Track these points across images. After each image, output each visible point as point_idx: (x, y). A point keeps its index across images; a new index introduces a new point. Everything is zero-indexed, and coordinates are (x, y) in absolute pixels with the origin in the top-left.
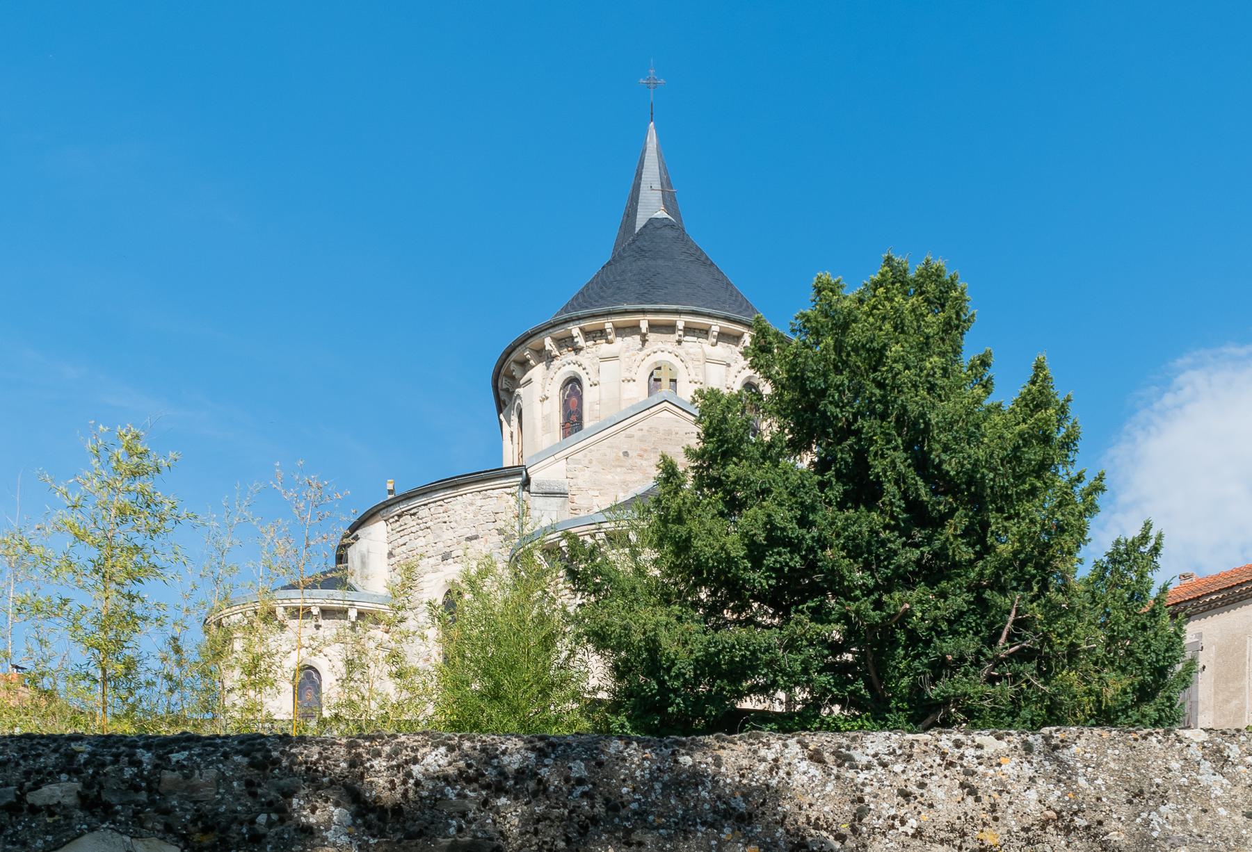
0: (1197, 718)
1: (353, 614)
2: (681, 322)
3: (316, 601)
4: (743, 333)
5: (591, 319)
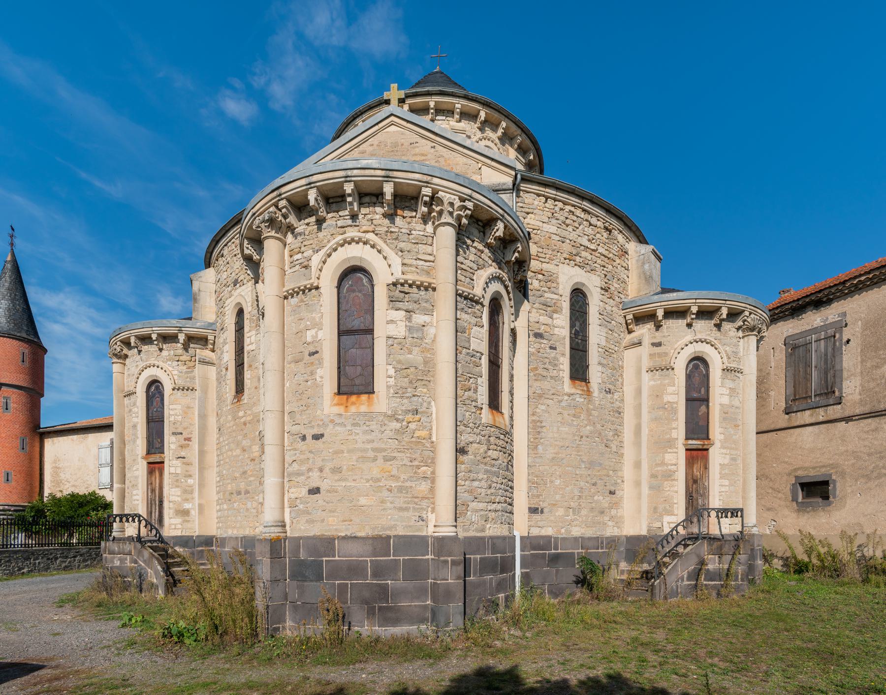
0: (842, 384)
1: (182, 337)
2: (432, 102)
3: (154, 329)
4: (479, 111)
5: (371, 113)
